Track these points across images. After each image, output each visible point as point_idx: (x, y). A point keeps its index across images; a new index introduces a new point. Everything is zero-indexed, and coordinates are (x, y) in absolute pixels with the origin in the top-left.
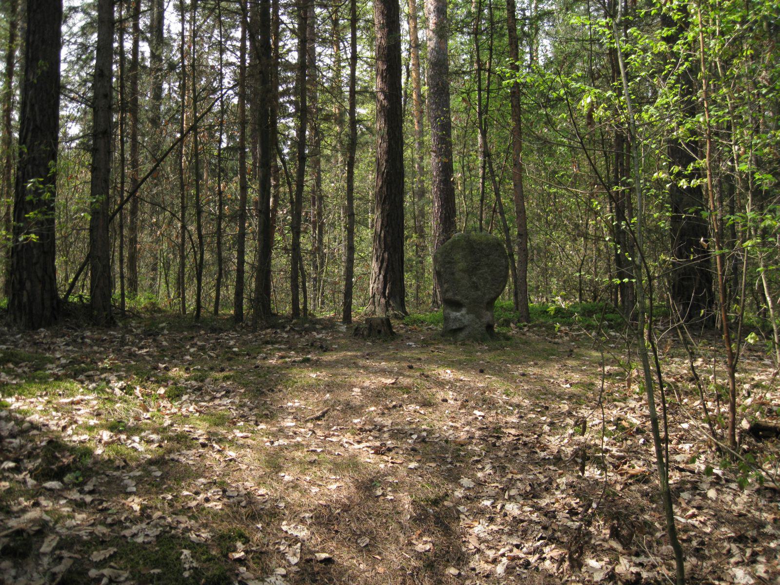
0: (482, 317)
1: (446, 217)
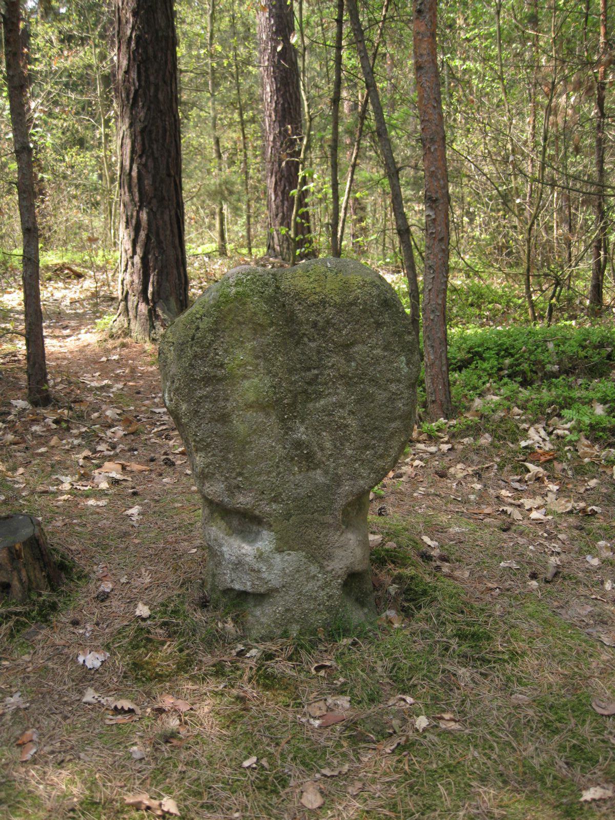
0: (330, 557)
1: (284, 110)
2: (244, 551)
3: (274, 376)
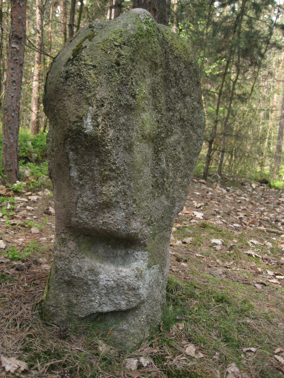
2: (123, 274)
3: (158, 111)
